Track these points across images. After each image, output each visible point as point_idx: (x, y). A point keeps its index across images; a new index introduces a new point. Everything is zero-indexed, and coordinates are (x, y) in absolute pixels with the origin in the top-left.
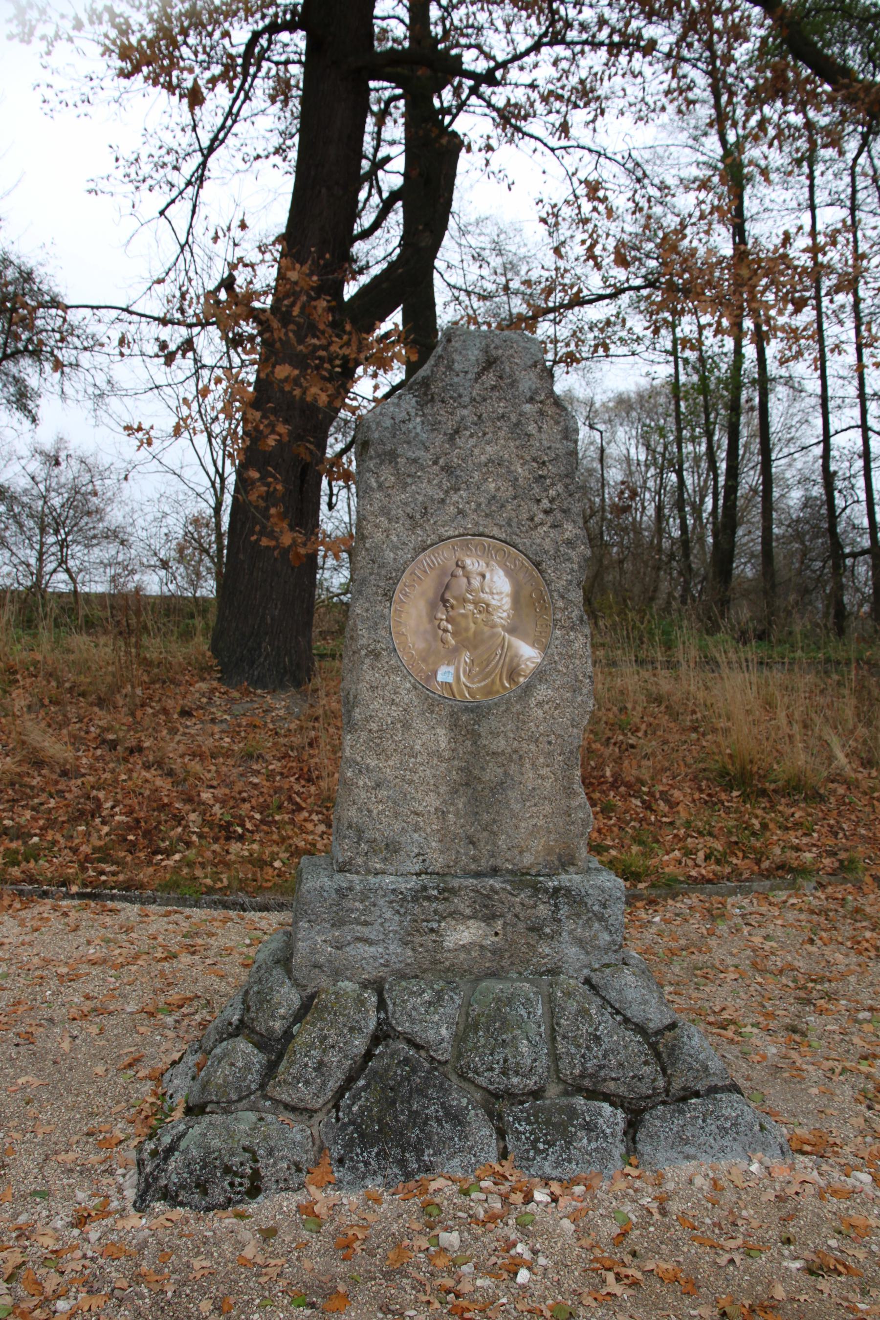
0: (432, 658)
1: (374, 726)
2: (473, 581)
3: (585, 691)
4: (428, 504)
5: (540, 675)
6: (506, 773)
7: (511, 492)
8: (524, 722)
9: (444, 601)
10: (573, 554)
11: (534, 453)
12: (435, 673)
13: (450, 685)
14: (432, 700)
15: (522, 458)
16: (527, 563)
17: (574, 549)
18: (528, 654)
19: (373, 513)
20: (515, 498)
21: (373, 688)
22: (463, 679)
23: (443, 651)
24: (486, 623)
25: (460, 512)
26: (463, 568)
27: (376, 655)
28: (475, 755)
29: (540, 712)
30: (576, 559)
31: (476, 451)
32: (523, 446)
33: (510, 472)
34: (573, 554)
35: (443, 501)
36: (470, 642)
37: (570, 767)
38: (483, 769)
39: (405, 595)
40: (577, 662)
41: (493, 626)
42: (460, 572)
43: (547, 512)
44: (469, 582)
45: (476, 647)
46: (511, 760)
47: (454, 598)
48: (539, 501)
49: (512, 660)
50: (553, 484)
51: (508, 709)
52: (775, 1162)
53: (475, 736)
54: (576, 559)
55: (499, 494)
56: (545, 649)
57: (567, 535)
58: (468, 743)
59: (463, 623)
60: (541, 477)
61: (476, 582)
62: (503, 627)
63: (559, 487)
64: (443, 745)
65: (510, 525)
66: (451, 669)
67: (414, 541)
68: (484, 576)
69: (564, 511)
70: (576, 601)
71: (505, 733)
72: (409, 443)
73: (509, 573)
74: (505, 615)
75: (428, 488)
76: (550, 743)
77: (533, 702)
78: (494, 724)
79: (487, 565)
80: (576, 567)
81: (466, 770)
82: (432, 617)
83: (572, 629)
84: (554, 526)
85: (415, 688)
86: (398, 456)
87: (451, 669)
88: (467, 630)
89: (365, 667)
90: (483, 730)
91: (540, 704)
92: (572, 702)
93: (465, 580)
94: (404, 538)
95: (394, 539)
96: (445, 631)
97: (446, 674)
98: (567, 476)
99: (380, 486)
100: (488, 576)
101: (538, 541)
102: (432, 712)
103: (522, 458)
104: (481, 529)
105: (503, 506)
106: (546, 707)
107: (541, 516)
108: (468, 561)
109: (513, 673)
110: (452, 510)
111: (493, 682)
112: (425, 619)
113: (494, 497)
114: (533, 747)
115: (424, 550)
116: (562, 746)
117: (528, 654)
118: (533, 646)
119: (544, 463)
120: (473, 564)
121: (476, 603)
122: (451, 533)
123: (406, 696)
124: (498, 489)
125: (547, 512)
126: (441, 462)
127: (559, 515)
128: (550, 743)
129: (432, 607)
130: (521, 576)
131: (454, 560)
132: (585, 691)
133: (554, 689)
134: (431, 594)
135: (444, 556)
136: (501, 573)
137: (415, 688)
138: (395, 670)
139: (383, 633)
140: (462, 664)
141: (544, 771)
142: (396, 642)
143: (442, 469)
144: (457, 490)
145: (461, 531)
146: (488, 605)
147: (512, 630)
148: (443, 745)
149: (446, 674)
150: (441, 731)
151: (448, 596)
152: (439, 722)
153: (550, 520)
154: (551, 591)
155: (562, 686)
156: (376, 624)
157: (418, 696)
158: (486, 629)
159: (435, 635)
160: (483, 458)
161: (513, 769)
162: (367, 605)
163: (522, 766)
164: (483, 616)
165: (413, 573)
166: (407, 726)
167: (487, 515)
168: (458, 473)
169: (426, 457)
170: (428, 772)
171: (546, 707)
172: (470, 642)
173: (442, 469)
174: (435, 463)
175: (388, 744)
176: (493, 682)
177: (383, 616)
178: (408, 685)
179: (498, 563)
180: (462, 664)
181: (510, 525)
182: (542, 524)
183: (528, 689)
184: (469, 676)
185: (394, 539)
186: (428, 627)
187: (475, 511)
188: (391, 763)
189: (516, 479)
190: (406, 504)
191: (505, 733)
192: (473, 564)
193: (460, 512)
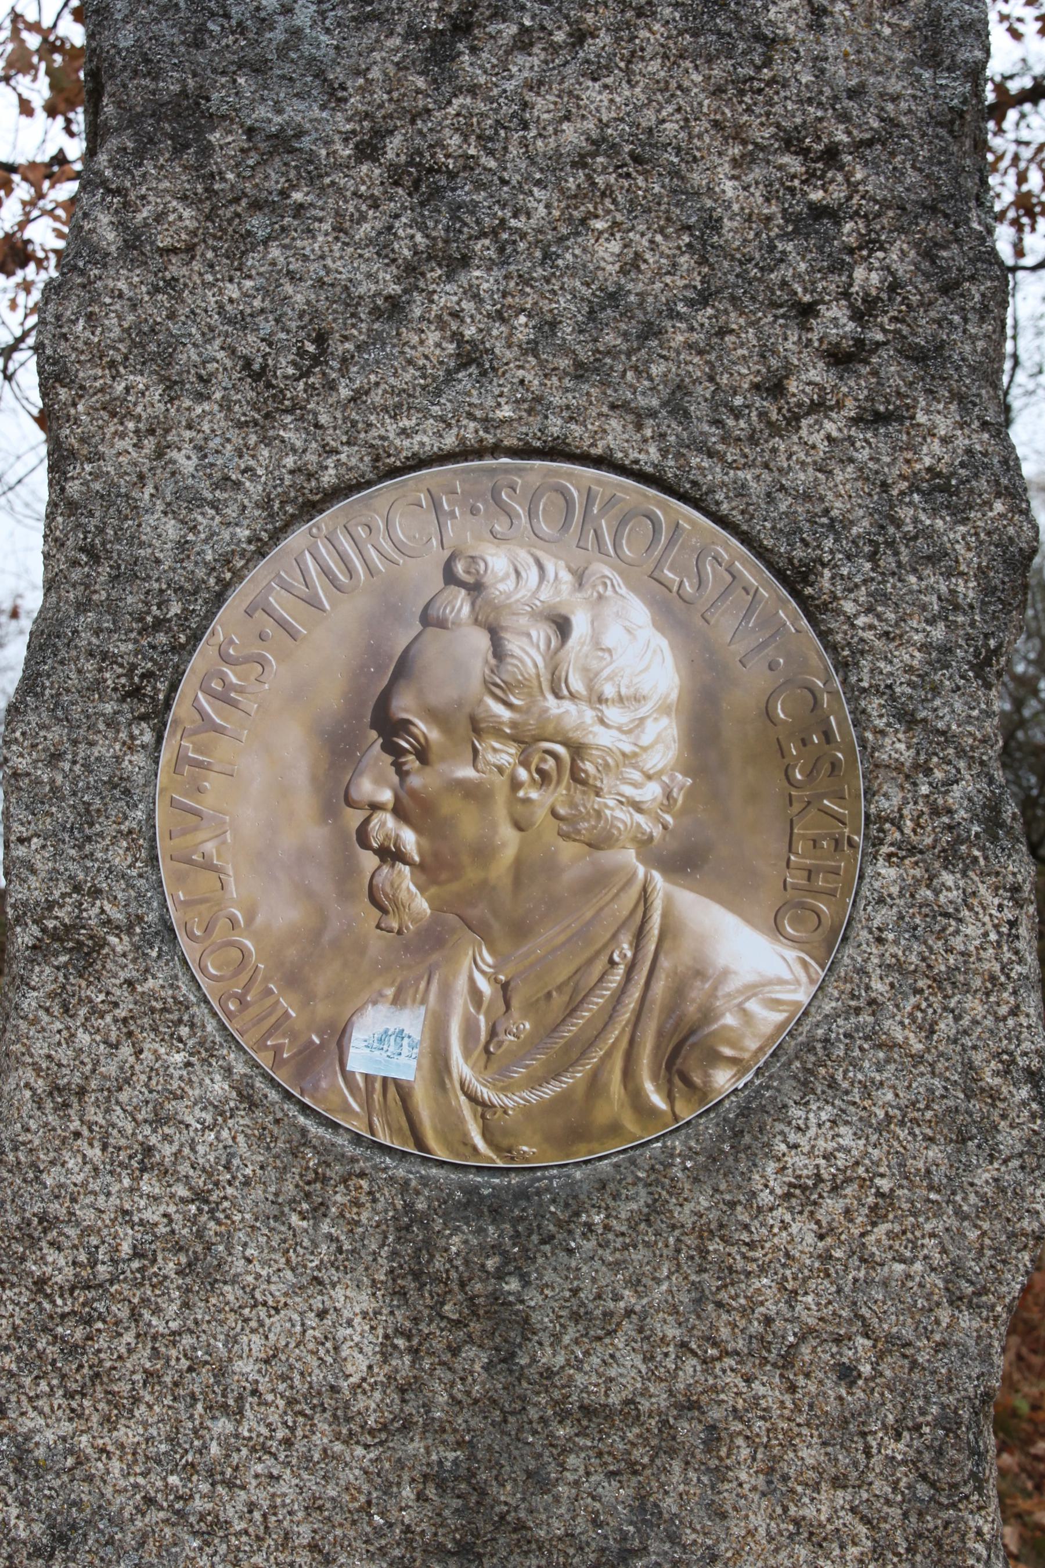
0: (325, 970)
1: (58, 1265)
2: (514, 645)
3: (1009, 1139)
4: (334, 321)
5: (803, 1059)
6: (643, 1507)
7: (688, 272)
8: (728, 1274)
9: (390, 728)
10: (957, 537)
11: (790, 112)
12: (339, 1037)
13: (404, 1092)
14: (320, 1153)
15: (738, 135)
16: (752, 573)
17: (959, 514)
18: (754, 968)
19: (98, 354)
20: (704, 298)
21: (63, 1096)
22: (461, 1066)
23: (376, 943)
24: (567, 825)
25: (471, 356)
26: (475, 588)
27: (85, 953)
28: (504, 1410)
29: (804, 1231)
30: (968, 558)
31: (543, 106)
32: (742, 86)
33: (683, 192)
34: (957, 537)
35: (394, 309)
36: (476, 902)
37: (946, 1495)
38: (538, 1481)
39: (224, 698)
40: (975, 1006)
41: (600, 842)
42: (460, 605)
43: (841, 358)
44: (498, 652)
45: (520, 930)
46: (667, 1444)
47: (434, 715)
48: (806, 312)
49: (679, 992)
50: (870, 244)
51: (654, 1210)
52: (875, 977)
53: (505, 1327)
54: (968, 558)
55: (634, 287)
56: (829, 943)
57: (931, 454)
58: (475, 1358)
59: (468, 826)
60: (818, 211)
61: (528, 649)
62: (644, 843)
63: (899, 256)
64: (357, 1365)
65: (679, 412)
66: (412, 1022)
67: (268, 467)
68: (562, 626)
69: (918, 356)
70: (969, 735)
71: (641, 1318)
72: (259, 68)
73: (673, 612)
74: (651, 792)
75: (336, 257)
76: (847, 1374)
77: (768, 1181)
78: (593, 1275)
79: (580, 578)
80: (967, 590)
81: (459, 1483)
82: (336, 796)
83: (949, 857)
84: (872, 418)
85: (249, 1100)
86: (214, 120)
87: (412, 1022)
88: (484, 852)
89: (30, 1002)
90: (541, 1301)
91: (802, 1194)
92: (952, 1186)
93: (481, 640)
94: (228, 462)
95: (186, 461)
96: (391, 854)
97: (384, 1042)
98: (931, 209)
99: (134, 243)
100: (581, 624)
101: (802, 478)
102: (319, 1211)
103: (738, 135)
104: (555, 426)
105: (650, 331)
106: (831, 1207)
107: (817, 373)
108: (497, 562)
109: (684, 1050)
110: (432, 345)
111: (595, 1084)
112: (304, 802)
113: (614, 297)
114: (768, 1390)
115: (310, 509)
116: (907, 1392)
117: (754, 968)
118: (777, 930)
119: (831, 155)
120: (516, 570)
121: (524, 740)
122: (425, 441)
123: (206, 1136)
124: (632, 265)
125: (841, 358)
126: (394, 147)
127: (895, 373)
128: (847, 1374)
129: (338, 752)
130: (726, 624)
131: (438, 556)
132: (1009, 1139)
133: (865, 1126)
134: (331, 695)
135: (389, 537)
136: (639, 612)
137: (249, 1100)
138: (169, 1017)
139: (119, 857)
140: (460, 1002)
141: (821, 1507)
142: (175, 895)
143: (395, 175)
144: (457, 263)
145: (470, 431)
146: (578, 750)
147: (684, 861)
148: (357, 1365)
149: (384, 1042)
150: (352, 1300)
151: (404, 706)
152: (345, 1259)
153: (854, 390)
154: (855, 693)
155: (905, 1116)
156: (88, 815)
157: (261, 1138)
158: (568, 850)
159: (347, 870)
160: (572, 135)
161: (678, 1486)
162: (56, 734)
163: (720, 1474)
164: (557, 796)
165: (258, 607)
166: (204, 1271)
167: (581, 371)
168: (464, 193)
169: (326, 129)
170: (286, 1488)
171: (831, 1207)
172: (476, 902)
173: (395, 175)
174: (368, 150)
175: (124, 1352)
176: (595, 1084)
177: (120, 786)
178: (219, 1087)
179: (625, 568)
180: (460, 1002)
181: (679, 412)
182: (818, 407)
183: (746, 1126)
184: (487, 1051)
185: (186, 461)
186: (316, 835)
187: (532, 349)
188: (128, 1434)
189: (713, 224)
190: (242, 322)
191: (641, 1318)
192: (516, 570)
193: (471, 356)
